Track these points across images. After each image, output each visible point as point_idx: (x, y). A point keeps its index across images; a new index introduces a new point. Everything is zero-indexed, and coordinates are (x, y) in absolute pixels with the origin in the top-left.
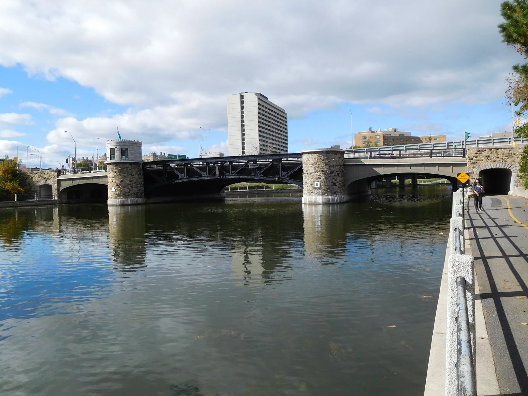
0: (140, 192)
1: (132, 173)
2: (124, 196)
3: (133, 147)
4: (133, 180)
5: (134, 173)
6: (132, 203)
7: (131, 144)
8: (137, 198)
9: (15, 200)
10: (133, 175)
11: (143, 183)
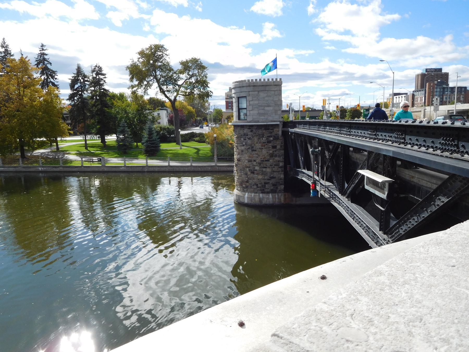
0: (272, 181)
2: (240, 188)
3: (256, 93)
4: (254, 159)
5: (258, 146)
6: (250, 202)
7: (249, 89)
8: (262, 193)
9: (311, 194)
10: (254, 149)
11: (281, 164)
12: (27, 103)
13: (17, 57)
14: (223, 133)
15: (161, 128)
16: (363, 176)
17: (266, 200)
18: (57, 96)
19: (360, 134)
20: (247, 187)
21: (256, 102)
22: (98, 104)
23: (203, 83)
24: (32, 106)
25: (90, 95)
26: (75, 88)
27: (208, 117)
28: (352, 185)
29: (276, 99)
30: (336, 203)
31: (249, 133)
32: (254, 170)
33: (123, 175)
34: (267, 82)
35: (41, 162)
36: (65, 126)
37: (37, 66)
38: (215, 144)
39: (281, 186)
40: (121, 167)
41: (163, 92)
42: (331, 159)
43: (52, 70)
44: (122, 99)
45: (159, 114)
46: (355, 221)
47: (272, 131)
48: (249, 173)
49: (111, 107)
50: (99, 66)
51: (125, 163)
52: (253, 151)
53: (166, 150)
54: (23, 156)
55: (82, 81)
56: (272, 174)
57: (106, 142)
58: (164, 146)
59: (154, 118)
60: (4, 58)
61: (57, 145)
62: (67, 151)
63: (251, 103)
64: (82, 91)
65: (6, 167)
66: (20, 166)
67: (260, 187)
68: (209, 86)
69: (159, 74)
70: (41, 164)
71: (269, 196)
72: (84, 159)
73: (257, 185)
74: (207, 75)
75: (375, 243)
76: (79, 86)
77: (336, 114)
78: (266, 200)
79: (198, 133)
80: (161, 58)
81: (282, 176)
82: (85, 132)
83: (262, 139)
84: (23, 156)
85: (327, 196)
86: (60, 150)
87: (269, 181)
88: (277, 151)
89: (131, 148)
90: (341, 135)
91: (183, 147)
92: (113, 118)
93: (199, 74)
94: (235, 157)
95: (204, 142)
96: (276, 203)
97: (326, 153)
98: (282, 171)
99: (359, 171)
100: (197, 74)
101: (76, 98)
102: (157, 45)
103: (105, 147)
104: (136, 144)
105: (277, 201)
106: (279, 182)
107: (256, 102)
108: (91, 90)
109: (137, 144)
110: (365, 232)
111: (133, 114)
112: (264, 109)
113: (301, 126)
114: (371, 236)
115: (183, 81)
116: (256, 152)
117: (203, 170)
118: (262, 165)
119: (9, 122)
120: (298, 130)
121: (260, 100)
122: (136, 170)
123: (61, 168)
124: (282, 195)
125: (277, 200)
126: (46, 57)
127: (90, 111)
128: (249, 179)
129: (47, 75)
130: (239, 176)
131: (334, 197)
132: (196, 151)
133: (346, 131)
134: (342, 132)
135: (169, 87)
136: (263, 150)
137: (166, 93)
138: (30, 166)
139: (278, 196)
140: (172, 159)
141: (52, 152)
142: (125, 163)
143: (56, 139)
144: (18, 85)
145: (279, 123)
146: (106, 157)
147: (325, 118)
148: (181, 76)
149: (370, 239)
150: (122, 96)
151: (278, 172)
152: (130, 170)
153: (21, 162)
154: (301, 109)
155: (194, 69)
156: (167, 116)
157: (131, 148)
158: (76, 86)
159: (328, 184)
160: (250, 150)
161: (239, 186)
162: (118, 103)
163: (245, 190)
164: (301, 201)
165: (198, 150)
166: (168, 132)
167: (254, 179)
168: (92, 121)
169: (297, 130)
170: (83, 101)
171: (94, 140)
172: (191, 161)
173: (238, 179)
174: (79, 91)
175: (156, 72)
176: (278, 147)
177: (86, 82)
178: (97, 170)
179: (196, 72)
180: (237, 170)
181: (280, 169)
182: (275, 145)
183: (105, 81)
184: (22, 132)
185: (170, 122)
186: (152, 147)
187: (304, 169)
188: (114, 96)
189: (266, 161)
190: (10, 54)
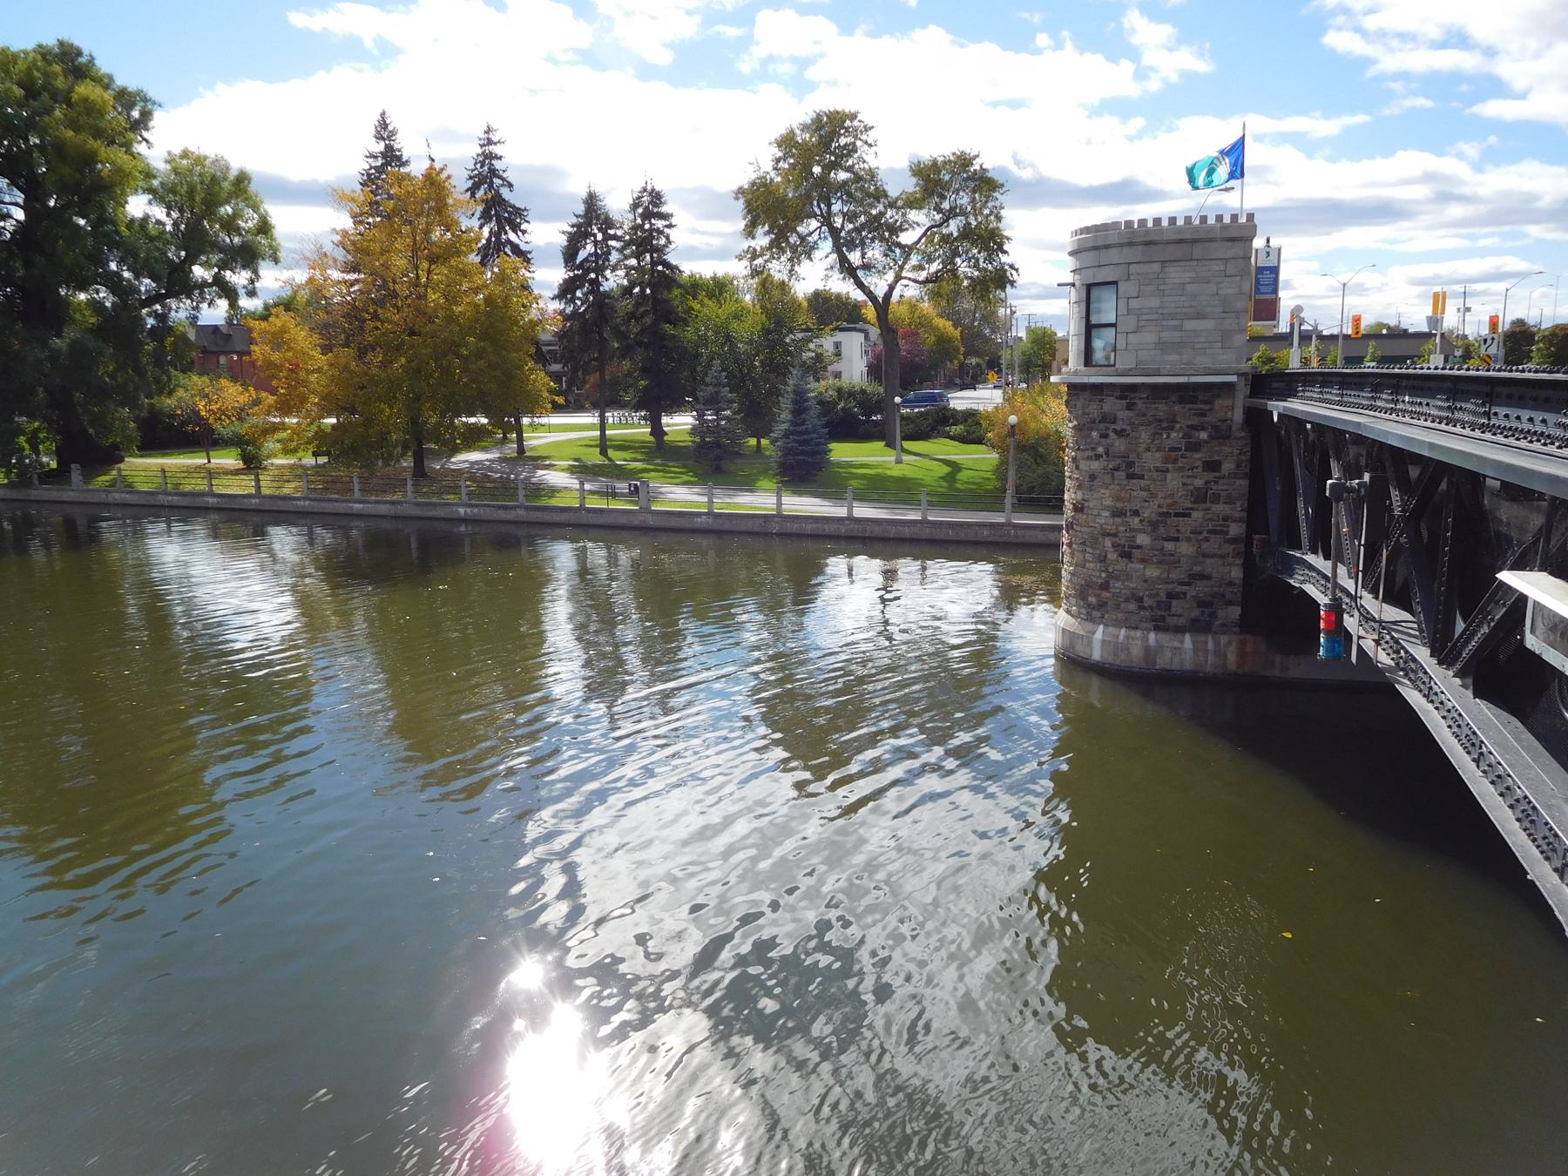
0: (1199, 589)
1: (1133, 457)
2: (1080, 607)
3: (1156, 267)
5: (1152, 460)
6: (1110, 659)
7: (1136, 253)
8: (1157, 629)
10: (1137, 471)
11: (1235, 529)
12: (435, 310)
13: (417, 168)
14: (1043, 412)
15: (839, 390)
16: (1523, 599)
17: (1168, 654)
18: (525, 287)
19: (1526, 426)
20: (1102, 605)
21: (1154, 302)
22: (645, 313)
23: (991, 241)
24: (451, 318)
25: (625, 282)
26: (578, 262)
27: (1005, 356)
28: (1479, 626)
29: (1230, 291)
30: (1417, 693)
31: (1122, 414)
32: (1131, 547)
33: (704, 541)
34: (1196, 229)
35: (464, 491)
36: (540, 380)
37: (473, 195)
38: (1011, 450)
39: (1231, 608)
40: (699, 514)
41: (849, 270)
42: (1413, 518)
43: (513, 207)
44: (721, 294)
45: (837, 345)
46: (1484, 772)
47: (1206, 407)
48: (1112, 556)
49: (680, 321)
50: (653, 190)
51: (711, 502)
52: (1130, 477)
53: (850, 465)
54: (420, 472)
55: (600, 237)
56: (1196, 564)
57: (665, 434)
58: (842, 452)
59: (819, 357)
60: (380, 173)
61: (520, 440)
62: (547, 458)
63: (1134, 304)
64: (600, 270)
65: (370, 502)
66: (406, 500)
67: (1151, 608)
68: (1006, 247)
69: (841, 211)
70: (465, 498)
71: (1182, 642)
72: (587, 487)
73: (1140, 600)
74: (1003, 213)
75: (1556, 870)
76: (590, 255)
77: (1483, 348)
78: (1168, 654)
79: (962, 412)
80: (849, 155)
81: (1236, 573)
82: (603, 401)
83: (1168, 437)
84: (420, 472)
85: (1384, 658)
86: (527, 454)
87: (1185, 588)
88: (1221, 481)
89: (736, 453)
90: (1450, 428)
91: (906, 458)
92: (689, 357)
93: (974, 208)
94: (1066, 497)
95: (979, 441)
96: (1208, 669)
97: (1395, 494)
98: (1237, 555)
99: (1505, 576)
100: (969, 208)
101: (579, 294)
102: (838, 113)
103: (660, 450)
104: (753, 441)
105: (1210, 664)
106: (1223, 596)
107: (1154, 302)
108: (626, 267)
109: (759, 442)
110: (1518, 820)
111: (750, 342)
112: (1180, 329)
113: (1314, 392)
114: (1540, 842)
115: (919, 232)
116: (1143, 483)
117: (962, 537)
118: (1162, 530)
119: (384, 364)
120: (1303, 406)
121: (1167, 293)
122: (742, 526)
123: (521, 512)
124: (1230, 643)
125: (1211, 659)
126: (497, 164)
127: (620, 335)
128: (1111, 576)
129: (499, 223)
130: (1076, 565)
131: (1409, 666)
132: (946, 470)
133: (1475, 413)
134: (1457, 415)
135: (869, 254)
136: (1169, 476)
137: (860, 273)
138: (434, 500)
139: (1217, 643)
140: (862, 497)
141: (502, 460)
142: (711, 502)
143: (518, 421)
144: (415, 250)
145: (1234, 378)
146: (656, 482)
147: (1435, 363)
148: (914, 215)
149: (1536, 852)
150: (719, 288)
151: (1223, 557)
152: (727, 526)
153: (410, 488)
154: (1349, 331)
155: (957, 192)
156: (866, 352)
157: (736, 453)
158: (582, 255)
159: (1391, 613)
160: (1121, 475)
161: (1073, 601)
162: (707, 308)
163: (1096, 614)
164: (1296, 669)
165: (955, 467)
166: (861, 404)
167: (1129, 577)
168: (626, 365)
169: (1296, 405)
170: (602, 302)
171: (632, 426)
172: (924, 503)
173: (1072, 574)
174: (587, 271)
175: (829, 206)
176: (1228, 466)
177: (610, 243)
178: (623, 520)
179: (964, 200)
180: (1070, 545)
181: (1229, 548)
182: (1217, 458)
183: (667, 238)
184: (418, 398)
185: (874, 371)
186: (803, 453)
187: (1315, 552)
188: (695, 287)
189: (1177, 515)
190: (399, 158)
